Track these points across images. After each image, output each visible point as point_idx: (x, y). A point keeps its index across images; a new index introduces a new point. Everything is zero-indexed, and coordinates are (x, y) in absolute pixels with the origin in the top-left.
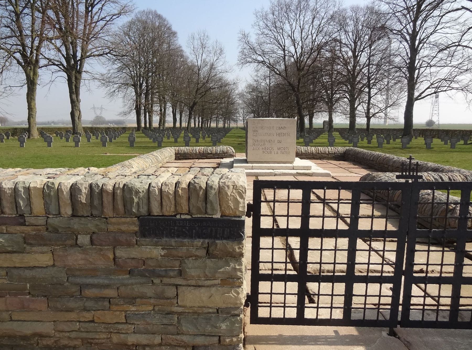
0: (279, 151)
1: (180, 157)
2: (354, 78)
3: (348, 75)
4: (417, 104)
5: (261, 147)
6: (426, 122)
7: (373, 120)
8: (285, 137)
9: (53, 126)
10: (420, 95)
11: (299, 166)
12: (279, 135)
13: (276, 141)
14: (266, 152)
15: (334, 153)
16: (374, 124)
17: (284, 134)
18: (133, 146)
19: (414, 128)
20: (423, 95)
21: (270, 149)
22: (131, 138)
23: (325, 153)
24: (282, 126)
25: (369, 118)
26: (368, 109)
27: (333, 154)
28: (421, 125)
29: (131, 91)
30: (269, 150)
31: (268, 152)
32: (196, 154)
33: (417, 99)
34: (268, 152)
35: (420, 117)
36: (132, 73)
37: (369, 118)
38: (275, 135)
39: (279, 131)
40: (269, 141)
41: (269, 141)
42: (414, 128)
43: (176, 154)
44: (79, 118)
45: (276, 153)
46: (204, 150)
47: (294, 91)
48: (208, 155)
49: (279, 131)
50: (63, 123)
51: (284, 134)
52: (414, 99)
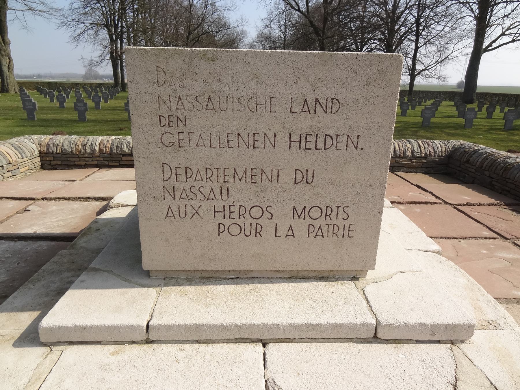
0: (301, 226)
1: (52, 161)
2: (395, 21)
3: (387, 18)
4: (485, 57)
5: (207, 206)
6: (458, 84)
7: (419, 81)
8: (332, 152)
9: (36, 79)
10: (490, 45)
11: (408, 327)
12: (304, 141)
13: (287, 176)
14: (235, 230)
15: (426, 157)
16: (421, 86)
17: (331, 140)
18: (33, 119)
19: (478, 91)
20: (495, 45)
21: (256, 212)
22: (27, 104)
23: (405, 156)
24: (322, 94)
25: (413, 76)
26: (414, 64)
27: (421, 157)
28: (451, 86)
29: (104, 33)
30: (248, 221)
31: (242, 229)
32: (92, 155)
33: (486, 50)
34: (242, 229)
35: (489, 77)
36: (104, 9)
37: (413, 76)
38: (282, 142)
39: (304, 123)
40: (252, 176)
41: (252, 176)
42: (478, 91)
43: (42, 155)
44: (9, 68)
45: (283, 231)
46: (112, 144)
47: (318, 35)
48: (124, 158)
49: (304, 123)
50: (51, 77)
51: (331, 140)
52: (482, 50)
